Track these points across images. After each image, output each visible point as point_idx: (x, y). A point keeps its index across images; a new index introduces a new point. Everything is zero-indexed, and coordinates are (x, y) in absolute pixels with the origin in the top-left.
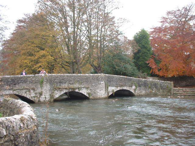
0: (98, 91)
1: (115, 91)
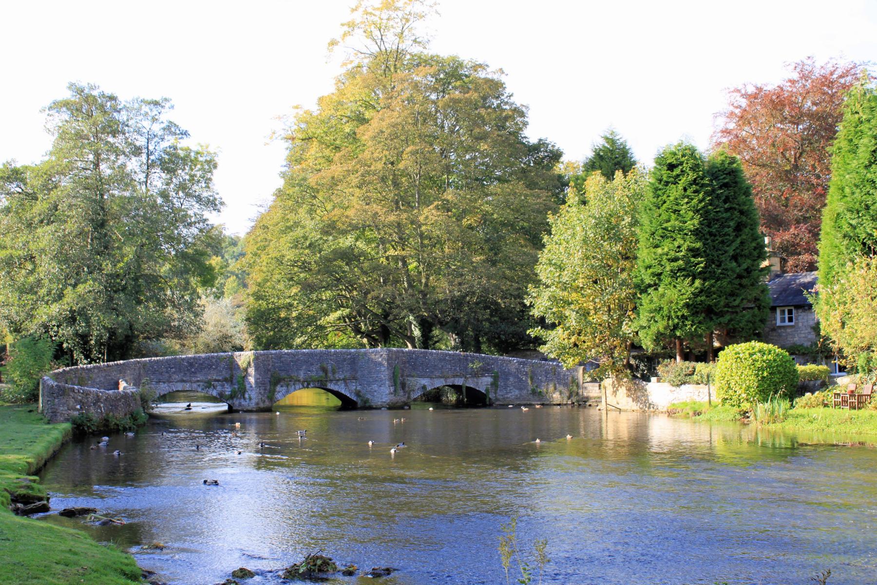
0: (375, 387)
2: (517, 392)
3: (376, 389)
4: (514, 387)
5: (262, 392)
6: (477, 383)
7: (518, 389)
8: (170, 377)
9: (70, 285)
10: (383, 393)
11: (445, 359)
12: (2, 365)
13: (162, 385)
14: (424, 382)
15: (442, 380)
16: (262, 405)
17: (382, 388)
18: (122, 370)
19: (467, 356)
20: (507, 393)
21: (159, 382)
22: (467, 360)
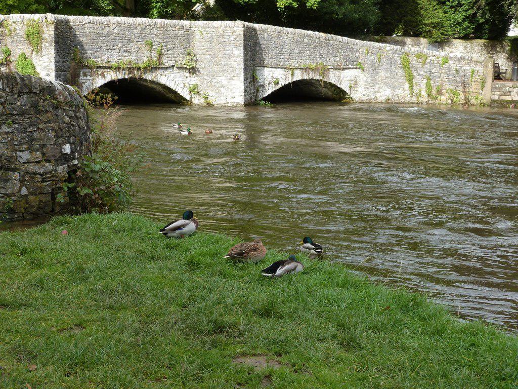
1: (282, 83)
3: (225, 83)
4: (385, 83)
7: (390, 87)
17: (232, 82)
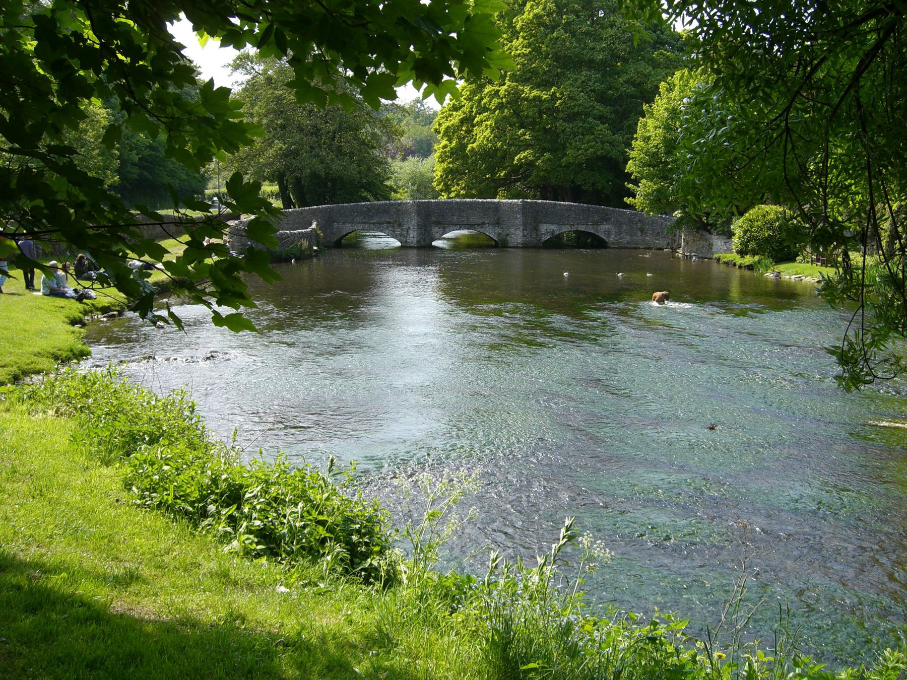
2: (628, 238)
5: (423, 232)
6: (597, 229)
7: (629, 235)
8: (353, 219)
9: (387, 142)
10: (517, 236)
11: (571, 209)
12: (617, 675)
13: (347, 225)
14: (553, 227)
15: (568, 226)
16: (423, 243)
18: (314, 213)
19: (589, 208)
20: (621, 238)
21: (344, 223)
22: (589, 210)
